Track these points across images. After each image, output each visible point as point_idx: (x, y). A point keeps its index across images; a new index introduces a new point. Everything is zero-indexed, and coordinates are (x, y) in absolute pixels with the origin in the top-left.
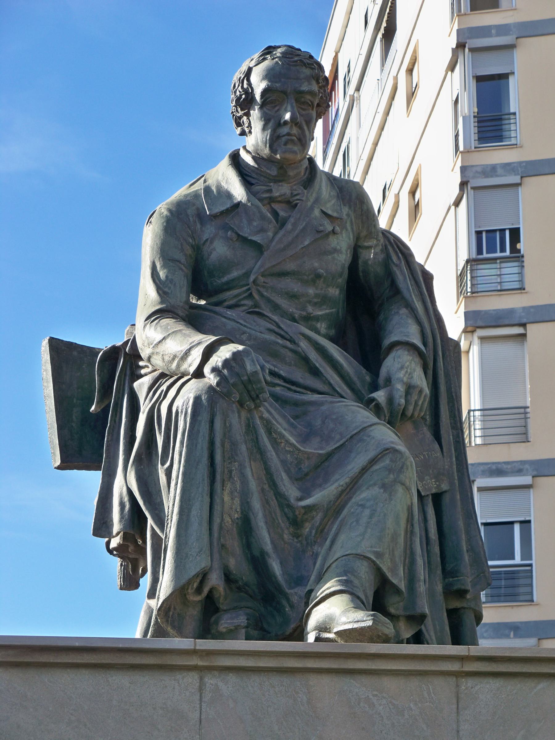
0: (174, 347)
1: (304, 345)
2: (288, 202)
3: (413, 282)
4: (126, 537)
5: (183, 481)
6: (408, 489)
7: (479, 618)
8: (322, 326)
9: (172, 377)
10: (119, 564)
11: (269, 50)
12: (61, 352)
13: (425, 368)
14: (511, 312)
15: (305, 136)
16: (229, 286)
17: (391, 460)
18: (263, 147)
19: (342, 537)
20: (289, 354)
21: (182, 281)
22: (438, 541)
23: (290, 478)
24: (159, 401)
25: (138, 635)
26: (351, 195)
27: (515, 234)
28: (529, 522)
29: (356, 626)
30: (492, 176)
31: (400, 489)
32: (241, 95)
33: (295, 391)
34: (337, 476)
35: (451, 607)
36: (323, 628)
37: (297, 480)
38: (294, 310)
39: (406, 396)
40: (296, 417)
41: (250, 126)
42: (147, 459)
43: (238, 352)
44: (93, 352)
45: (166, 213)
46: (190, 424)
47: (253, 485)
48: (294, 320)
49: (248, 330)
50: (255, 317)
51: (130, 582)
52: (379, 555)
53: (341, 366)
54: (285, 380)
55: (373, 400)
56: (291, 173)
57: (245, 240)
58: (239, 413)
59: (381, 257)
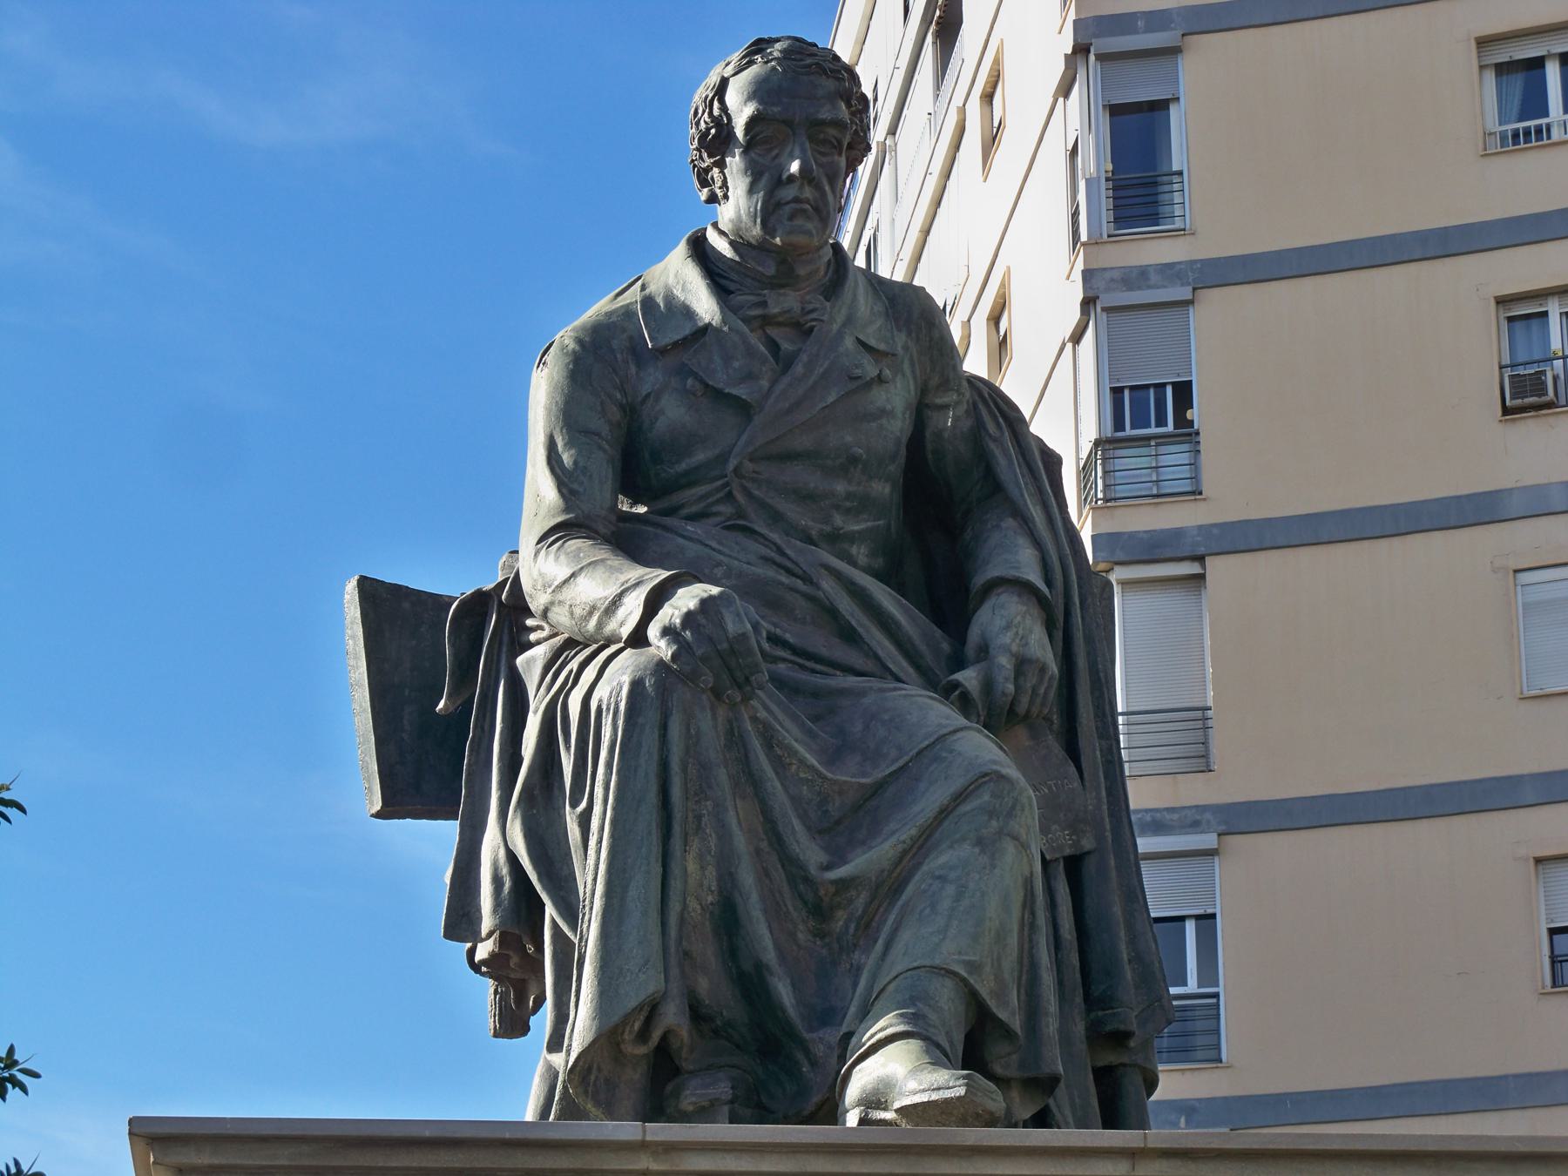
0: (593, 588)
1: (828, 585)
2: (797, 325)
3: (1025, 471)
4: (506, 939)
5: (613, 835)
6: (1025, 846)
7: (1151, 1084)
8: (860, 552)
9: (587, 646)
10: (492, 990)
11: (759, 46)
12: (380, 601)
13: (1050, 626)
14: (1178, 534)
15: (826, 204)
16: (689, 479)
17: (993, 795)
18: (750, 224)
19: (905, 936)
20: (802, 602)
21: (603, 472)
22: (1075, 943)
23: (809, 829)
24: (566, 691)
25: (530, 1115)
26: (912, 312)
27: (1183, 392)
28: (1213, 916)
29: (935, 1096)
30: (1140, 288)
31: (1010, 848)
32: (708, 130)
33: (814, 671)
34: (892, 826)
35: (1100, 1064)
36: (874, 1100)
37: (820, 832)
38: (810, 523)
39: (1016, 679)
40: (816, 719)
41: (725, 185)
42: (543, 798)
43: (711, 598)
44: (441, 602)
45: (572, 346)
46: (624, 731)
47: (740, 842)
48: (809, 540)
49: (726, 560)
50: (740, 537)
51: (513, 1023)
52: (974, 967)
53: (897, 624)
54: (795, 650)
55: (956, 685)
56: (802, 271)
57: (718, 396)
58: (713, 709)
59: (967, 424)
